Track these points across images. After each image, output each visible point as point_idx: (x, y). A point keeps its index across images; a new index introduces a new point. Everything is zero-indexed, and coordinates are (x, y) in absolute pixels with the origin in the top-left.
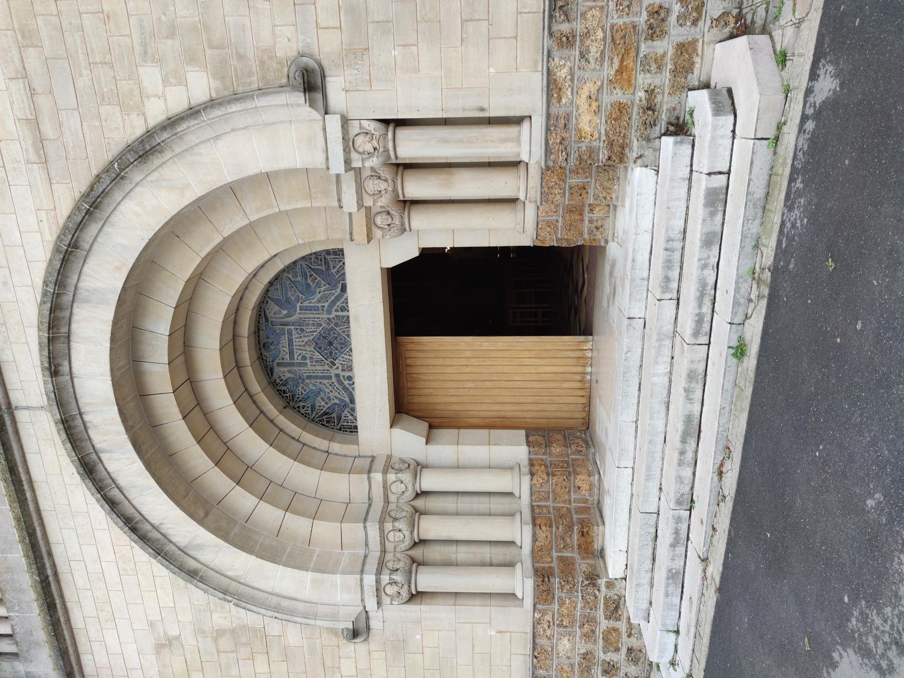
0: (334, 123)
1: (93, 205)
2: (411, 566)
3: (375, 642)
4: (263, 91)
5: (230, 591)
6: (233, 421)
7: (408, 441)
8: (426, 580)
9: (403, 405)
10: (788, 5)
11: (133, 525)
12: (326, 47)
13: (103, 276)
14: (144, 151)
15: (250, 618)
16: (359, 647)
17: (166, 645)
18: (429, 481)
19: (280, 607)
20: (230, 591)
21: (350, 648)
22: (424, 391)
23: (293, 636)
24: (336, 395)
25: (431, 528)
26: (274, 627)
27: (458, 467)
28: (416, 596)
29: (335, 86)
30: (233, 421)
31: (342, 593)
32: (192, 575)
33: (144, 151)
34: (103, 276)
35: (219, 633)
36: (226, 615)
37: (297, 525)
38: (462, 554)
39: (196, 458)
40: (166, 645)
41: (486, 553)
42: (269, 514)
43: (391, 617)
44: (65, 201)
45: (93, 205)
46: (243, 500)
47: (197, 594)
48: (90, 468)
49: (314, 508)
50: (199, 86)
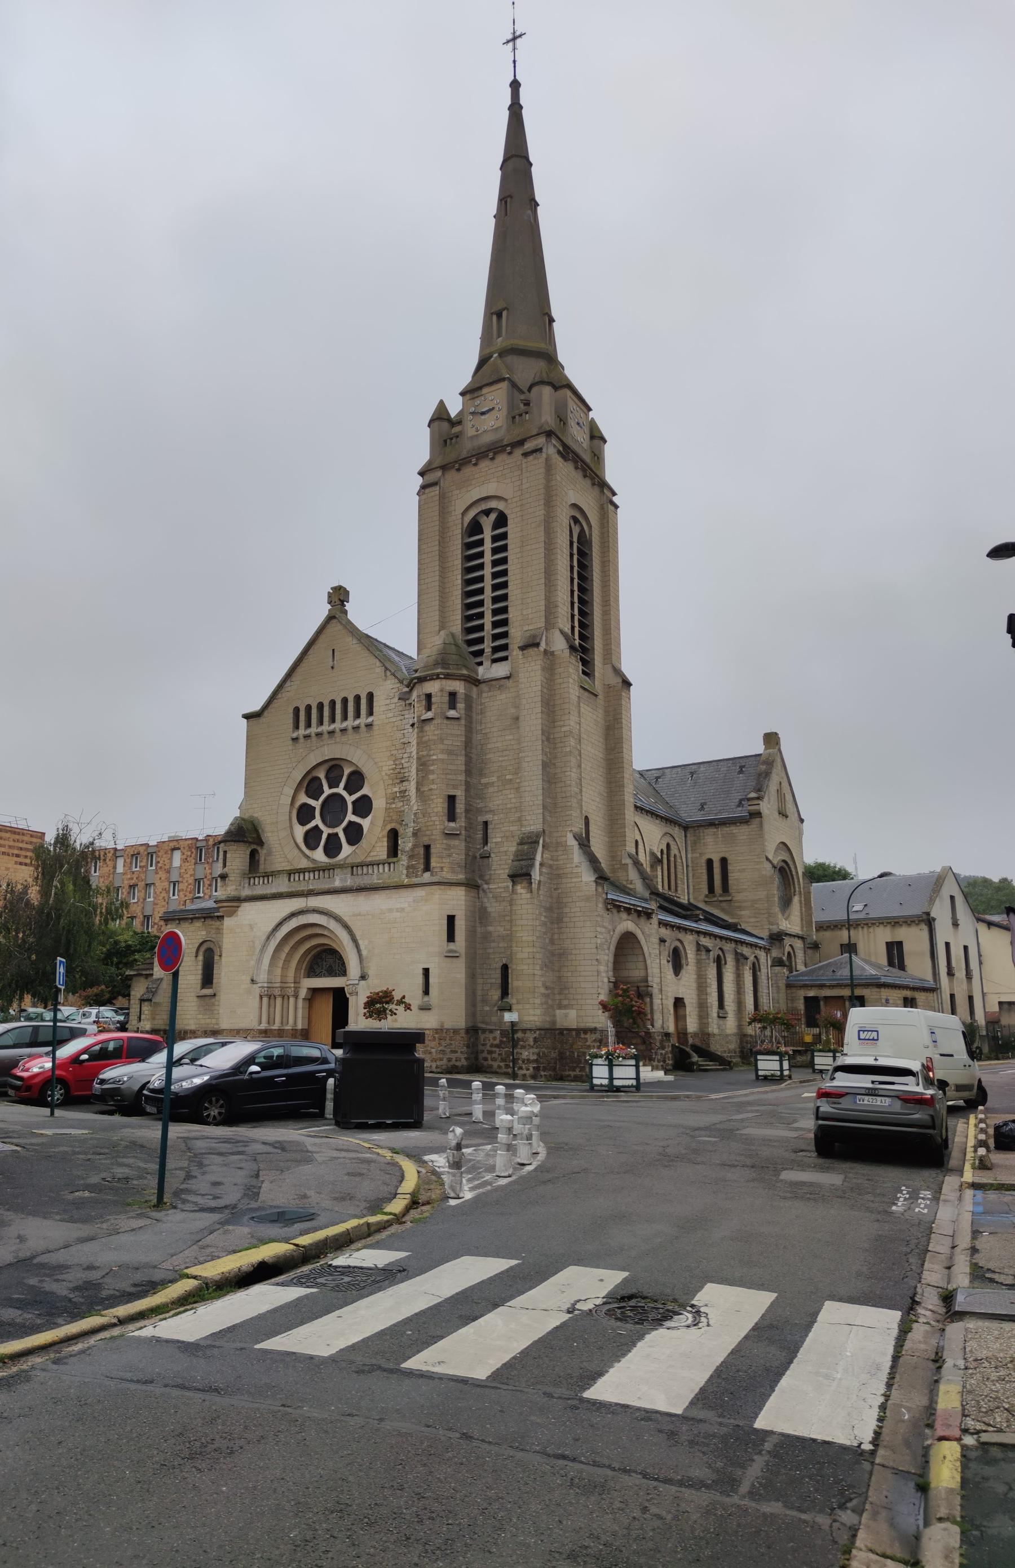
0: (356, 982)
1: (346, 927)
2: (269, 996)
3: (250, 985)
4: (362, 968)
5: (264, 947)
6: (308, 945)
7: (303, 993)
8: (265, 1000)
9: (315, 992)
10: (2, 842)
11: (280, 924)
12: (370, 981)
13: (333, 925)
14: (355, 940)
15: (258, 950)
16: (249, 981)
17: (251, 927)
18: (292, 1000)
19: (259, 961)
20: (264, 947)
21: (249, 979)
22: (573, 957)
23: (252, 963)
24: (318, 971)
25: (279, 1001)
26: (255, 958)
27: (296, 1008)
28: (261, 997)
29: (363, 982)
30: (308, 945)
31: (263, 977)
32: (268, 938)
33: (355, 940)
34: (333, 925)
35: (253, 942)
36: (258, 947)
37: (280, 964)
38: (272, 1010)
39: (298, 937)
40: (251, 927)
41: (272, 1016)
42: (283, 956)
43: (256, 990)
44: (346, 919)
45: (346, 927)
46: (287, 949)
47: (264, 937)
48: (293, 915)
49: (285, 967)
50: (364, 953)
